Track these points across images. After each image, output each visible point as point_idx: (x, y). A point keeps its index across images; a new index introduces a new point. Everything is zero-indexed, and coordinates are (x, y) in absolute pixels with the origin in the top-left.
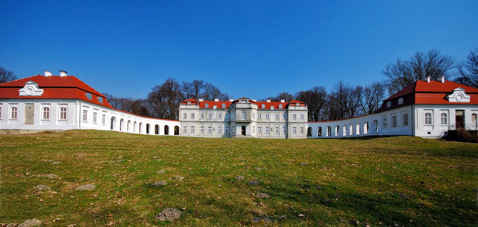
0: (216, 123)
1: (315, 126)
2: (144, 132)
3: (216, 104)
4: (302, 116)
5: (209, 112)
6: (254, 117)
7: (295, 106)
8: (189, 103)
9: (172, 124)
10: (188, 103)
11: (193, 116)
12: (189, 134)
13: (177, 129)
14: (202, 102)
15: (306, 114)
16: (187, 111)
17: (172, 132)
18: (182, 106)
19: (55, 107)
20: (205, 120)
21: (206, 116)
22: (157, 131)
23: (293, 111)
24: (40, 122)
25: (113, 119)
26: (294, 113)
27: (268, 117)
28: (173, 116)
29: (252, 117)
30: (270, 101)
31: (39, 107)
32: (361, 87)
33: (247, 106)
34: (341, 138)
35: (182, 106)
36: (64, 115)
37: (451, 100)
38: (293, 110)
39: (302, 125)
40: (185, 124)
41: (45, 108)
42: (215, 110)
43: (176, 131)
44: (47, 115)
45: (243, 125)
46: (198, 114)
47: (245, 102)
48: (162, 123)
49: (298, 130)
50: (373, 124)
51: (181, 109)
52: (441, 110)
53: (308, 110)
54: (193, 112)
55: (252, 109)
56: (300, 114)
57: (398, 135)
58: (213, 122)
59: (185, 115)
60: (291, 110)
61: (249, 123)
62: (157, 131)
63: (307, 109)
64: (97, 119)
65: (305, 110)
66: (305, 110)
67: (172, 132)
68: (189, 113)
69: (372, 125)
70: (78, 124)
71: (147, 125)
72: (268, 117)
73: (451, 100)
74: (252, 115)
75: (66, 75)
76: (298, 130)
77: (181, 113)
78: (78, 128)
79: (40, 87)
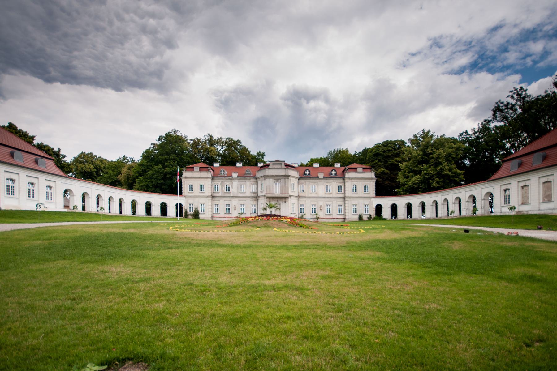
0: (237, 199)
1: (386, 202)
4: (366, 188)
5: (227, 182)
7: (356, 172)
9: (172, 201)
10: (359, 170)
11: (202, 188)
13: (179, 207)
18: (185, 174)
20: (220, 195)
21: (222, 189)
23: (353, 180)
26: (355, 182)
28: (172, 188)
29: (290, 190)
30: (318, 166)
32: (467, 119)
33: (282, 172)
35: (185, 174)
38: (352, 178)
39: (366, 202)
43: (42, 229)
46: (208, 184)
47: (279, 166)
48: (156, 199)
50: (484, 199)
51: (186, 178)
55: (290, 178)
56: (364, 181)
58: (233, 197)
60: (349, 178)
61: (285, 199)
63: (374, 176)
65: (372, 178)
68: (196, 185)
69: (483, 201)
71: (132, 202)
72: (314, 191)
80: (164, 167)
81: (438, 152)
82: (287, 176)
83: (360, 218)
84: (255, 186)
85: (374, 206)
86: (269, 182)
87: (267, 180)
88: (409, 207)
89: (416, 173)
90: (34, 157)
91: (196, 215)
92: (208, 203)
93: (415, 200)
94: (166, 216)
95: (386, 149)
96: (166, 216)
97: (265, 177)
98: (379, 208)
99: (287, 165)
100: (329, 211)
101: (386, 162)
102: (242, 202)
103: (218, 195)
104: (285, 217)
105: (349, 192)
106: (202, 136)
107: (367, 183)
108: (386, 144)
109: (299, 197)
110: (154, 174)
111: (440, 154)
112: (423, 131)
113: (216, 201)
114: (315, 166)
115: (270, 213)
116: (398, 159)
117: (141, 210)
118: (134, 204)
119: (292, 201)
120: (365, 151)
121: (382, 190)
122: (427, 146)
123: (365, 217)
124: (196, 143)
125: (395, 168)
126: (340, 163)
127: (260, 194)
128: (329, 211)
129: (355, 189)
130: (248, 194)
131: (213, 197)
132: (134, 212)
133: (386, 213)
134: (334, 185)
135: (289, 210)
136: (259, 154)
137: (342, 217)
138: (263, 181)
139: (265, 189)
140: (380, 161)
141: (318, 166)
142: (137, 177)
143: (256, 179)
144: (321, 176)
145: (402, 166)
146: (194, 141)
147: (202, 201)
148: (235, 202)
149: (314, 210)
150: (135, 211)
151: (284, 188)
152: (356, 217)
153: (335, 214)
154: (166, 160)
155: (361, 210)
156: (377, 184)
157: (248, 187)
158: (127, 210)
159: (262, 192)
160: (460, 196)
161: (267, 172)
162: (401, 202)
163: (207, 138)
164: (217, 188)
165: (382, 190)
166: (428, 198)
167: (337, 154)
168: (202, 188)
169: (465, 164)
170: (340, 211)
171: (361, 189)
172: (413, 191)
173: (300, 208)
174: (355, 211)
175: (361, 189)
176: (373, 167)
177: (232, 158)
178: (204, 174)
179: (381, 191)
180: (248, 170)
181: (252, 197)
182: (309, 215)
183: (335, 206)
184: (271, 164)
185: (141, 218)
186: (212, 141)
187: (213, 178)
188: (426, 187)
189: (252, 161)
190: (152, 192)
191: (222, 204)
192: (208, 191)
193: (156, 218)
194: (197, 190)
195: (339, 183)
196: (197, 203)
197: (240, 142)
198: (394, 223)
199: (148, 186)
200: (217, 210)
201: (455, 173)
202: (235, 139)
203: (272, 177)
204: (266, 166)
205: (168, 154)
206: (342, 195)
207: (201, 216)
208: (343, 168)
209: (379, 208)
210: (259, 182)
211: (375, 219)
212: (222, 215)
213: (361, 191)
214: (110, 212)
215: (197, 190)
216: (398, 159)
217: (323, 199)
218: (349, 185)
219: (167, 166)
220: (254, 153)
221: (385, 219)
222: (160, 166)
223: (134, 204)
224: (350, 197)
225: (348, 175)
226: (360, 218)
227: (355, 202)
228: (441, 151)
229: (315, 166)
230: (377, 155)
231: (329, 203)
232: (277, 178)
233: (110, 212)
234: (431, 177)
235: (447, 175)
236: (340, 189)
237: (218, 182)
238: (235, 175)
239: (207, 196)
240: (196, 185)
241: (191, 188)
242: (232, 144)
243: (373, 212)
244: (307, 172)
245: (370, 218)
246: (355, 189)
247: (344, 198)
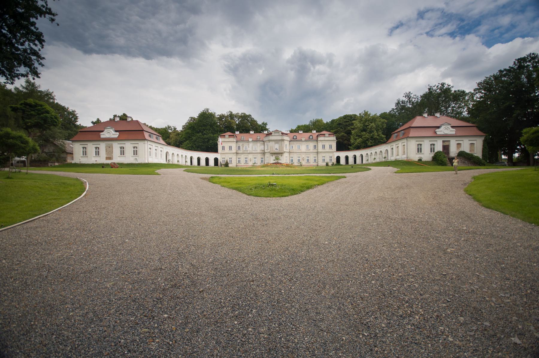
1: (342, 155)
2: (189, 163)
4: (331, 147)
5: (246, 144)
6: (286, 148)
7: (325, 136)
8: (227, 136)
9: (212, 156)
10: (326, 135)
11: (230, 148)
13: (216, 160)
19: (129, 146)
20: (241, 152)
22: (199, 163)
25: (167, 153)
26: (324, 143)
28: (214, 149)
29: (284, 148)
31: (116, 146)
33: (280, 138)
36: (135, 153)
37: (102, 136)
39: (331, 155)
41: (121, 148)
47: (278, 134)
48: (203, 155)
54: (230, 144)
56: (329, 142)
58: (249, 153)
61: (282, 154)
62: (199, 163)
68: (227, 146)
70: (147, 159)
72: (299, 148)
73: (102, 136)
74: (284, 146)
75: (446, 68)
78: (147, 162)
79: (116, 131)
80: (203, 133)
81: (371, 124)
82: (283, 140)
83: (327, 164)
84: (263, 146)
86: (271, 144)
87: (271, 143)
89: (360, 136)
90: (149, 134)
91: (227, 165)
92: (234, 158)
93: (358, 153)
95: (345, 120)
97: (269, 141)
98: (338, 158)
99: (283, 133)
100: (308, 160)
101: (345, 129)
102: (255, 156)
103: (240, 152)
105: (320, 149)
106: (225, 112)
107: (331, 143)
108: (346, 117)
109: (290, 152)
110: (197, 139)
111: (372, 126)
112: (365, 111)
113: (239, 156)
114: (300, 132)
115: (288, 162)
116: (352, 127)
117: (203, 163)
118: (199, 159)
119: (286, 155)
120: (333, 121)
121: (341, 147)
122: (366, 121)
123: (330, 164)
124: (222, 117)
125: (349, 133)
126: (318, 127)
127: (266, 151)
128: (308, 160)
129: (324, 147)
130: (259, 151)
131: (237, 153)
133: (343, 161)
134: (311, 145)
135: (285, 159)
136: (263, 123)
137: (316, 164)
138: (268, 144)
140: (341, 128)
142: (185, 141)
145: (353, 132)
146: (220, 116)
147: (230, 156)
148: (250, 156)
149: (299, 160)
151: (281, 147)
152: (325, 164)
153: (312, 162)
154: (204, 130)
155: (327, 160)
157: (259, 147)
159: (267, 150)
160: (376, 151)
161: (271, 138)
162: (350, 154)
163: (229, 113)
164: (239, 148)
165: (341, 147)
166: (364, 152)
167: (315, 122)
168: (230, 148)
170: (315, 160)
171: (327, 147)
172: (358, 148)
174: (324, 160)
175: (327, 147)
177: (244, 126)
178: (231, 139)
180: (259, 136)
181: (261, 153)
182: (296, 163)
183: (312, 158)
185: (194, 167)
186: (231, 116)
187: (237, 142)
188: (365, 145)
189: (260, 129)
190: (186, 149)
191: (242, 158)
192: (234, 150)
193: (202, 167)
194: (227, 150)
195: (314, 143)
196: (227, 158)
197: (250, 116)
198: (347, 166)
199: (192, 147)
200: (239, 162)
201: (381, 137)
202: (247, 114)
203: (273, 140)
204: (270, 134)
205: (204, 126)
206: (316, 151)
207: (230, 165)
208: (317, 134)
209: (338, 158)
210: (265, 144)
211: (336, 165)
212: (243, 164)
213: (327, 148)
215: (227, 150)
216: (352, 127)
218: (320, 145)
219: (205, 134)
220: (260, 123)
221: (342, 165)
222: (201, 134)
223: (199, 159)
224: (321, 152)
225: (319, 139)
226: (327, 164)
227: (324, 155)
228: (373, 124)
229: (300, 132)
230: (339, 124)
232: (276, 141)
234: (368, 140)
235: (376, 139)
236: (315, 147)
237: (240, 144)
240: (227, 147)
241: (223, 148)
242: (245, 117)
243: (334, 161)
244: (295, 137)
245: (333, 164)
246: (324, 147)
247: (317, 153)
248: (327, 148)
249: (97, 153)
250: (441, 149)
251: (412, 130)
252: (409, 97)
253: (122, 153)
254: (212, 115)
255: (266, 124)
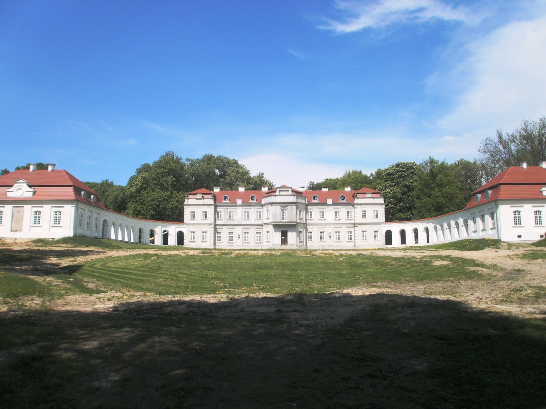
1: (396, 228)
3: (240, 196)
4: (376, 214)
9: (173, 229)
12: (199, 243)
13: (180, 236)
14: (217, 193)
15: (381, 211)
16: (197, 208)
17: (172, 241)
24: (490, 231)
27: (322, 214)
28: (179, 218)
34: (54, 200)
39: (376, 228)
40: (193, 229)
42: (240, 206)
44: (37, 220)
45: (284, 229)
48: (159, 229)
49: (370, 235)
51: (188, 205)
52: (511, 206)
53: (216, 253)
56: (372, 207)
57: (414, 234)
59: (193, 213)
64: (61, 221)
65: (381, 204)
66: (381, 204)
67: (172, 241)
68: (199, 211)
72: (322, 214)
76: (370, 235)
77: (187, 212)
85: (384, 233)
88: (403, 233)
94: (405, 244)
96: (405, 244)
98: (389, 234)
104: (504, 242)
112: (430, 158)
126: (358, 183)
129: (364, 214)
132: (403, 241)
134: (343, 211)
139: (271, 216)
141: (326, 190)
143: (262, 206)
144: (329, 202)
150: (493, 241)
156: (386, 211)
158: (158, 241)
162: (409, 227)
169: (219, 170)
173: (307, 235)
176: (376, 191)
179: (390, 217)
184: (278, 190)
209: (389, 234)
213: (370, 218)
214: (428, 242)
217: (332, 227)
220: (253, 173)
224: (360, 224)
225: (356, 201)
227: (364, 228)
231: (338, 230)
233: (428, 242)
236: (349, 214)
238: (239, 202)
239: (210, 224)
246: (364, 214)
248: (370, 218)
249: (57, 221)
250: (289, 234)
251: (502, 187)
252: (500, 137)
253: (37, 220)
254: (177, 161)
255: (263, 174)
